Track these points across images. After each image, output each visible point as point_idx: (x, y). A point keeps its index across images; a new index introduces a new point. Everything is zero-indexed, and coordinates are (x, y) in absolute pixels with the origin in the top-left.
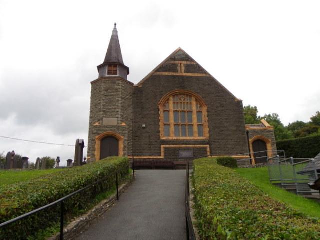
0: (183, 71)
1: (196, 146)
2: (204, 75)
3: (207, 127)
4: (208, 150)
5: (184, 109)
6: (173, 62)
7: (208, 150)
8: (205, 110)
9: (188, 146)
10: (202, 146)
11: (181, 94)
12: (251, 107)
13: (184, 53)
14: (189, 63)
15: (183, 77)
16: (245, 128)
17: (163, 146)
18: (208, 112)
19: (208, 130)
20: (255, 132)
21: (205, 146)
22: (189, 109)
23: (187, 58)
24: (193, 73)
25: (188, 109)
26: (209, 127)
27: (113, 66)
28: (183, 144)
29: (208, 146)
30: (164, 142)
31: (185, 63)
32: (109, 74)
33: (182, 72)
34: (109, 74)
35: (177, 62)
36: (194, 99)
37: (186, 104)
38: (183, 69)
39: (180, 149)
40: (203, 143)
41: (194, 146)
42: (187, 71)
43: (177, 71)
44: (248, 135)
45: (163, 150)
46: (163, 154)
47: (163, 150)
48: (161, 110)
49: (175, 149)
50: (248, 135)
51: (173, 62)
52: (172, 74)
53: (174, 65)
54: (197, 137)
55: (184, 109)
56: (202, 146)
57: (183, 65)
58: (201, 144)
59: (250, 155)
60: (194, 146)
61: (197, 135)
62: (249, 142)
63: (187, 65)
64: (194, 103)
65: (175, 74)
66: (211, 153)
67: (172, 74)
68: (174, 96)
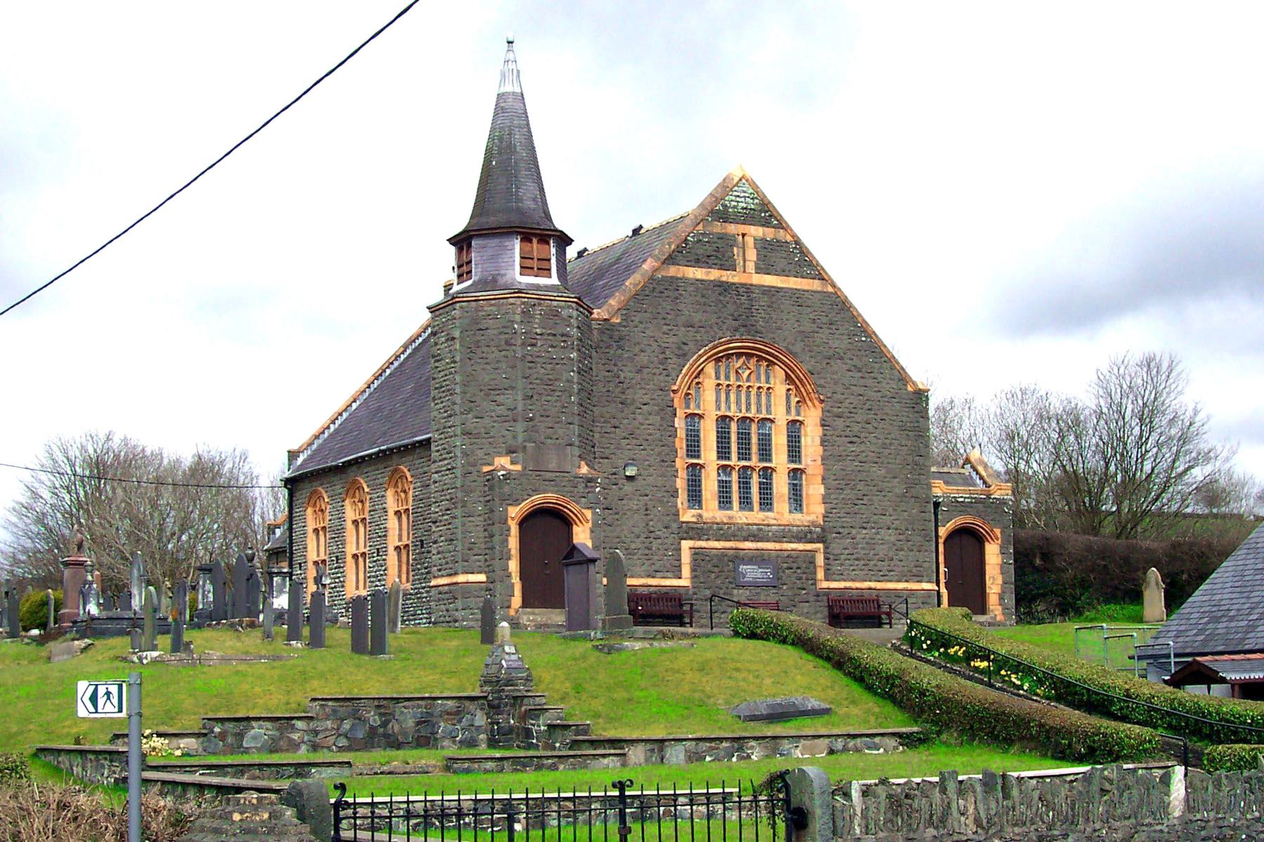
0: (751, 266)
1: (461, 578)
2: (816, 285)
3: (819, 479)
4: (820, 560)
5: (748, 410)
6: (718, 227)
7: (820, 560)
8: (812, 417)
9: (760, 545)
10: (801, 546)
11: (739, 355)
12: (148, 453)
13: (757, 193)
14: (769, 233)
15: (749, 288)
16: (929, 487)
17: (686, 544)
18: (823, 425)
19: (822, 490)
20: (958, 507)
21: (809, 546)
22: (764, 411)
23: (764, 214)
24: (783, 273)
25: (758, 411)
26: (823, 479)
27: (535, 241)
28: (746, 539)
29: (820, 546)
30: (696, 531)
31: (757, 231)
32: (525, 269)
33: (748, 273)
34: (525, 269)
35: (732, 229)
36: (779, 373)
37: (753, 392)
38: (752, 255)
39: (738, 558)
40: (803, 536)
41: (778, 546)
42: (764, 267)
43: (728, 264)
44: (936, 514)
45: (686, 558)
46: (686, 571)
47: (686, 558)
48: (680, 413)
49: (722, 556)
50: (936, 514)
51: (718, 227)
52: (714, 274)
53: (723, 237)
54: (782, 513)
55: (748, 410)
56: (801, 546)
57: (750, 241)
58: (799, 540)
59: (938, 585)
60: (778, 546)
61: (786, 507)
62: (937, 536)
63: (764, 240)
64: (780, 388)
65: (727, 276)
66: (827, 570)
67: (714, 274)
68: (718, 360)
